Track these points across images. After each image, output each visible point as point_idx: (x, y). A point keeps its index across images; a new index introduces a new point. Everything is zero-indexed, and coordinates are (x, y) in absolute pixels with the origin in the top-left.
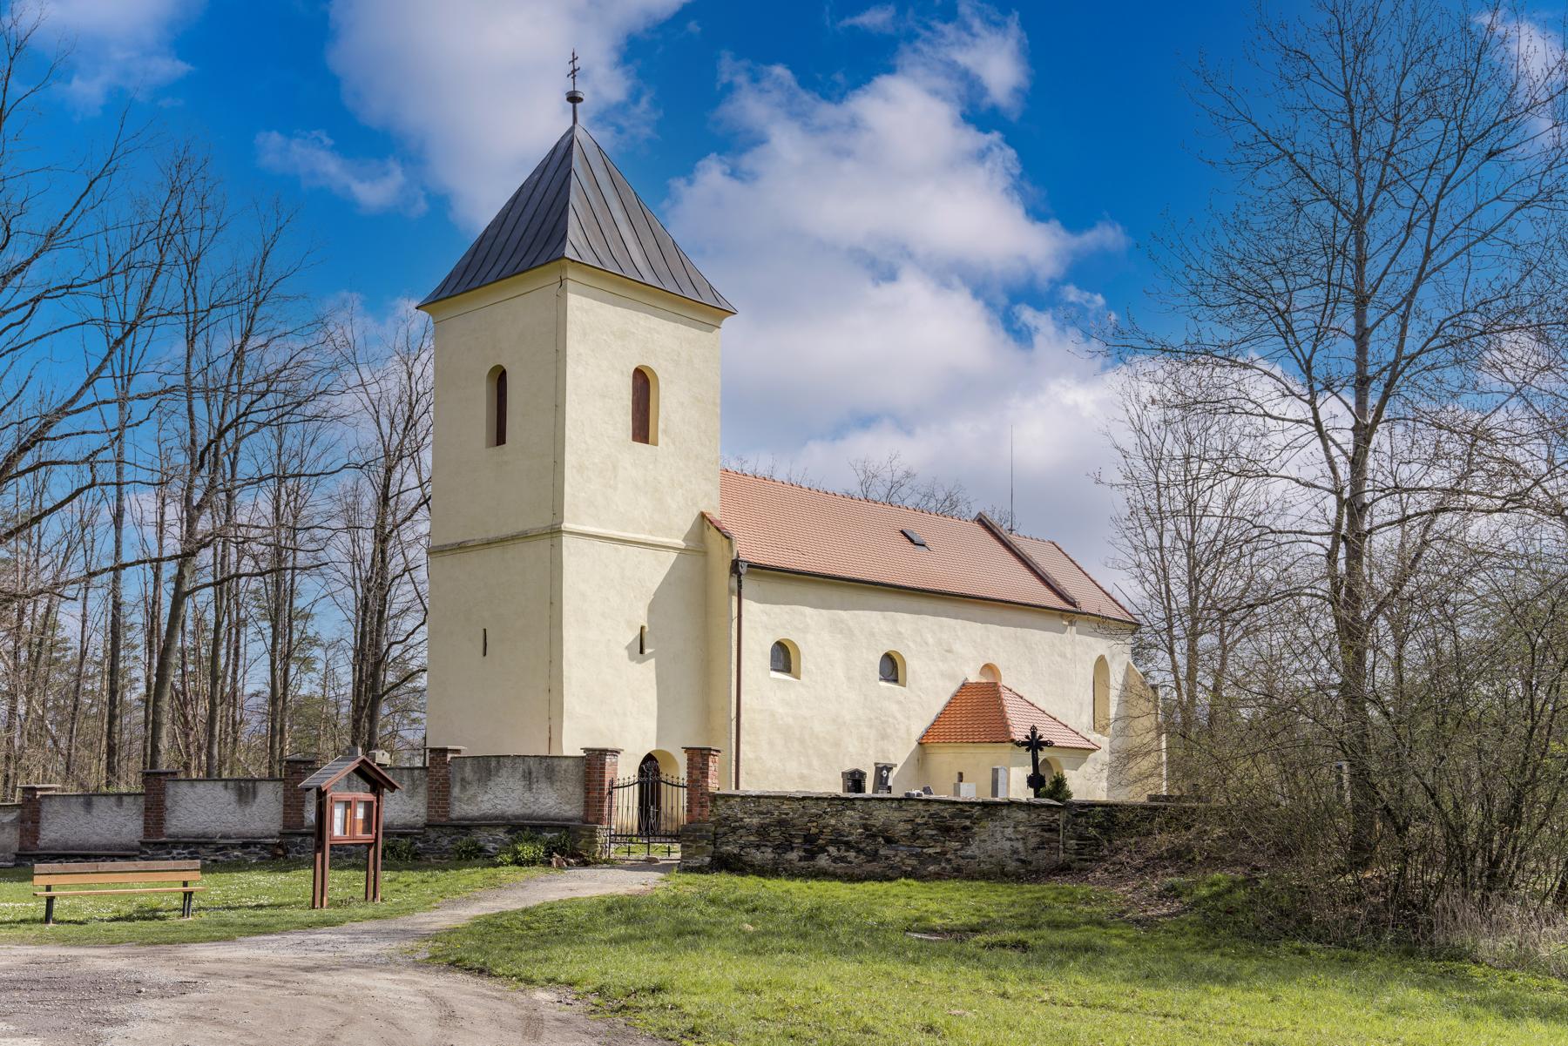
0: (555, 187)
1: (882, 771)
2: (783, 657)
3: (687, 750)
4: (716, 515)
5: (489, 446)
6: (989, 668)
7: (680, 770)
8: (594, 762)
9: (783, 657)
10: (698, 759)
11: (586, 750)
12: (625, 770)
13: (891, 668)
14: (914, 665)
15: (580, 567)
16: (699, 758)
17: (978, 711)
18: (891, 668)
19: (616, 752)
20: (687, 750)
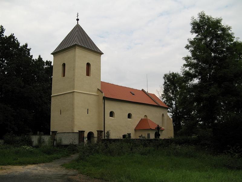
0: (82, 33)
1: (129, 135)
2: (112, 114)
3: (98, 131)
4: (100, 89)
5: (62, 77)
6: (145, 116)
7: (96, 135)
8: (81, 133)
9: (112, 114)
10: (99, 133)
11: (79, 131)
12: (86, 135)
13: (129, 116)
14: (133, 116)
15: (78, 100)
16: (100, 132)
17: (143, 125)
18: (129, 116)
19: (84, 131)
20: (98, 131)
